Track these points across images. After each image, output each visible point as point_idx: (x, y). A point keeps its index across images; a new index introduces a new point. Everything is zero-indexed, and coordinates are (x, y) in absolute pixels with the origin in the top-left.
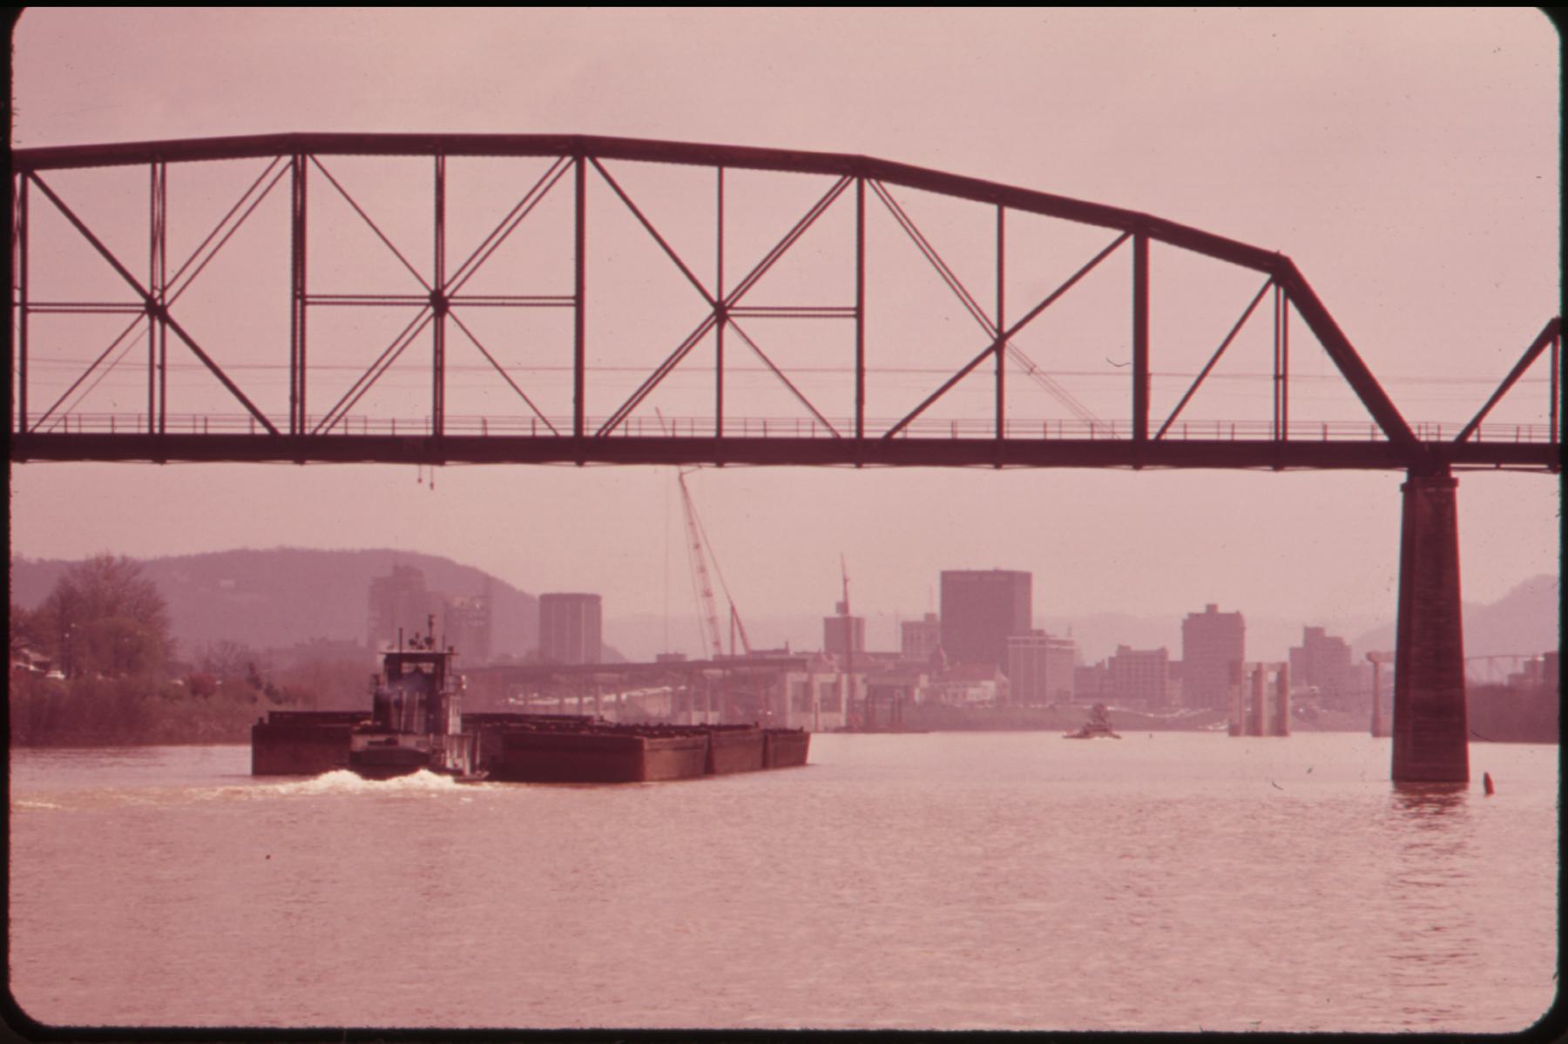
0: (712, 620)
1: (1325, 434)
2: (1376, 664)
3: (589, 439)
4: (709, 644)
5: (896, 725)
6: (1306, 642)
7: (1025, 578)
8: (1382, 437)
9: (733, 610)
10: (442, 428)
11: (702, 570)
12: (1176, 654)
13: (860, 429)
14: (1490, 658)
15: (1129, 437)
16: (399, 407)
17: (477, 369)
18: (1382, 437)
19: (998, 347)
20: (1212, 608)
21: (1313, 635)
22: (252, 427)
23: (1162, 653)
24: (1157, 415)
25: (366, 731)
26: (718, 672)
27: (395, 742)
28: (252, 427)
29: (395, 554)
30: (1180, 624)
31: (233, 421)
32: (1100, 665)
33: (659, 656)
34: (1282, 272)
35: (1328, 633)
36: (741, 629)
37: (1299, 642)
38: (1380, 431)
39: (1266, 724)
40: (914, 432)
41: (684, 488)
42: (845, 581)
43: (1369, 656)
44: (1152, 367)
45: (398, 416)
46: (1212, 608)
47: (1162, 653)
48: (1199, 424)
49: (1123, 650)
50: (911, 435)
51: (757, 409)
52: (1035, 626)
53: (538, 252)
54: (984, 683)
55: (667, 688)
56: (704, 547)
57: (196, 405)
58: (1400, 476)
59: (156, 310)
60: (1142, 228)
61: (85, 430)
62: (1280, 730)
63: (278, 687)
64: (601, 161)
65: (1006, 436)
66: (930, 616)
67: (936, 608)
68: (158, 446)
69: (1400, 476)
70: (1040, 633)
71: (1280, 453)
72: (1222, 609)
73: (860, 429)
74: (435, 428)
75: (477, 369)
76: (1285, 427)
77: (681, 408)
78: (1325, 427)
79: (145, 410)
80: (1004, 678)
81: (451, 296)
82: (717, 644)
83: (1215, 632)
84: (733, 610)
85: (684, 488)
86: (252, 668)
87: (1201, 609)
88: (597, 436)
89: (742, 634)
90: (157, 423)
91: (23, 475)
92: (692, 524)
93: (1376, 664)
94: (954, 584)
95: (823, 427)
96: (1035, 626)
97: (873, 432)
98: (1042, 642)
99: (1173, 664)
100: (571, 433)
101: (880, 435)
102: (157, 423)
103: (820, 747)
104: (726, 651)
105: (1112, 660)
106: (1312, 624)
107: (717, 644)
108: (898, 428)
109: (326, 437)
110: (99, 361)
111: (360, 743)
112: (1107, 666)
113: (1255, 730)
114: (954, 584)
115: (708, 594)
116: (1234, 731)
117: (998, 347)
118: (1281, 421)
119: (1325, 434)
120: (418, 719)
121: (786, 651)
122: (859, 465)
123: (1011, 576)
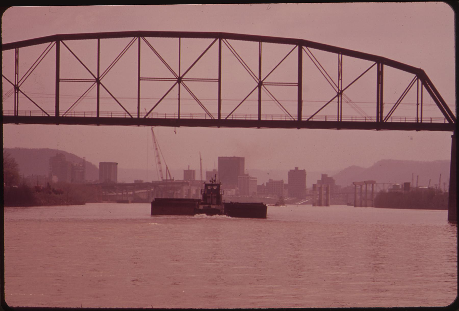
0: (161, 171)
1: (326, 119)
2: (355, 185)
3: (141, 118)
4: (160, 178)
5: (283, 204)
6: (322, 178)
7: (219, 158)
8: (447, 122)
9: (167, 168)
10: (301, 119)
11: (158, 156)
12: (286, 182)
13: (139, 115)
14: (384, 184)
15: (54, 115)
16: (87, 109)
17: (202, 99)
18: (447, 122)
19: (340, 94)
20: (297, 168)
21: (324, 176)
22: (445, 121)
23: (282, 181)
24: (385, 114)
25: (202, 204)
26: (162, 186)
27: (210, 207)
28: (445, 121)
29: (57, 151)
30: (287, 173)
31: (119, 113)
32: (263, 185)
33: (135, 181)
34: (421, 75)
35: (329, 176)
36: (169, 173)
37: (320, 179)
38: (446, 120)
39: (323, 203)
40: (314, 119)
41: (153, 132)
42: (201, 160)
43: (354, 183)
44: (303, 99)
45: (167, 113)
46: (297, 168)
47: (282, 181)
48: (396, 117)
49: (270, 180)
50: (313, 120)
51: (191, 110)
52: (246, 173)
53: (207, 68)
54: (232, 190)
55: (146, 191)
56: (158, 149)
57: (109, 109)
58: (452, 133)
59: (98, 81)
60: (381, 61)
61: (76, 116)
62: (327, 205)
63: (55, 189)
64: (63, 41)
65: (262, 119)
66: (214, 170)
67: (217, 168)
68: (98, 121)
69: (452, 133)
70: (247, 175)
71: (419, 126)
72: (299, 169)
73: (139, 115)
74: (56, 114)
75: (202, 99)
76: (341, 117)
77: (167, 110)
78: (326, 117)
79: (337, 115)
80: (238, 188)
81: (177, 78)
82: (162, 178)
83: (297, 176)
84: (167, 168)
85: (153, 132)
86: (48, 184)
87: (294, 169)
88: (145, 118)
89: (169, 173)
90: (340, 118)
91: (6, 127)
92: (155, 142)
93: (355, 185)
94: (222, 160)
95: (128, 114)
96: (246, 173)
97: (304, 119)
98: (248, 178)
99: (285, 185)
100: (217, 118)
101: (306, 120)
102: (340, 118)
103: (271, 210)
104: (165, 178)
105: (267, 183)
106: (324, 173)
107: (162, 178)
108: (310, 118)
109: (66, 117)
110: (123, 98)
111: (201, 207)
112: (265, 185)
113: (320, 205)
114: (222, 160)
115: (159, 163)
116: (314, 205)
117: (340, 94)
118: (16, 111)
119: (326, 119)
120: (215, 201)
121: (173, 180)
122: (219, 127)
123: (239, 158)
